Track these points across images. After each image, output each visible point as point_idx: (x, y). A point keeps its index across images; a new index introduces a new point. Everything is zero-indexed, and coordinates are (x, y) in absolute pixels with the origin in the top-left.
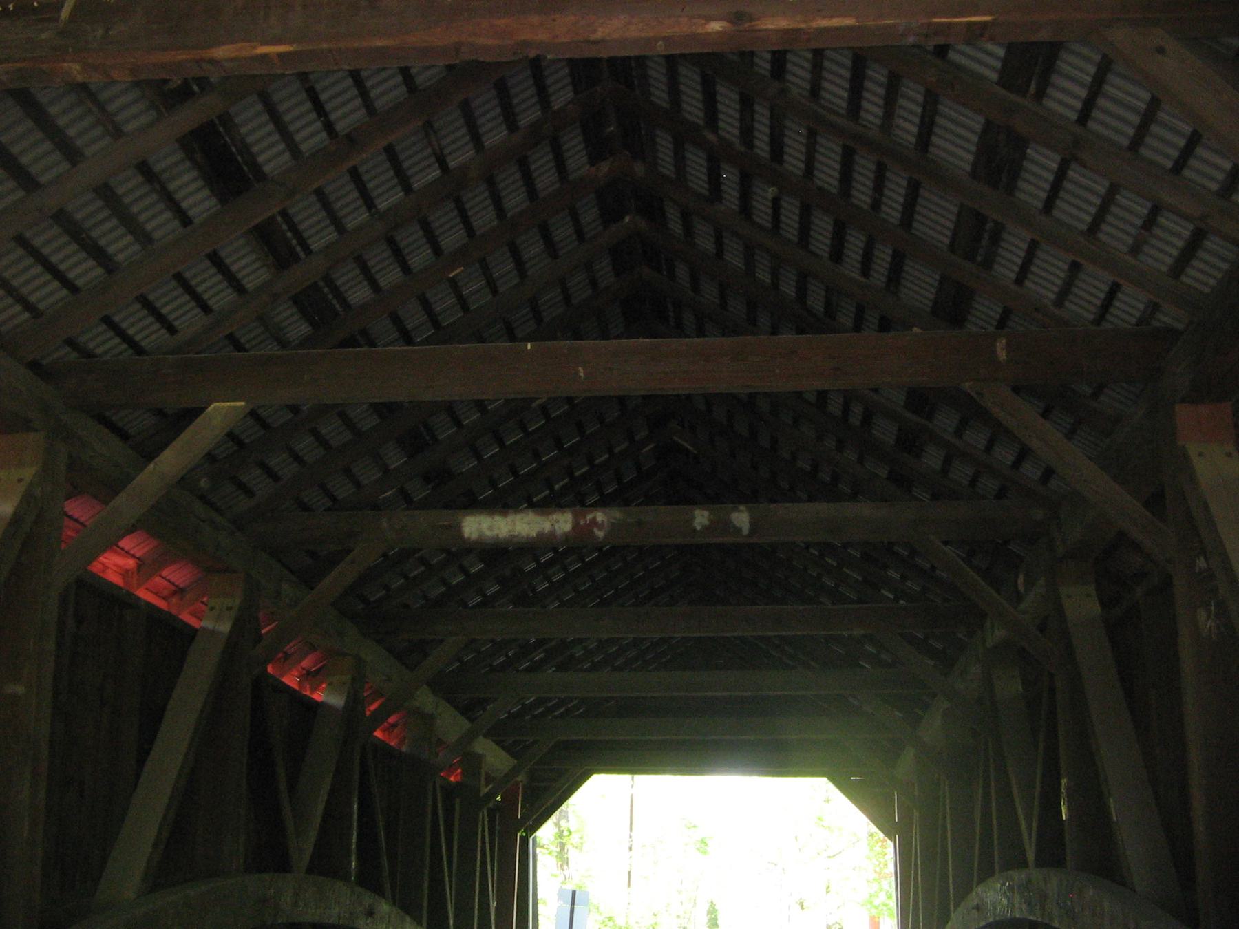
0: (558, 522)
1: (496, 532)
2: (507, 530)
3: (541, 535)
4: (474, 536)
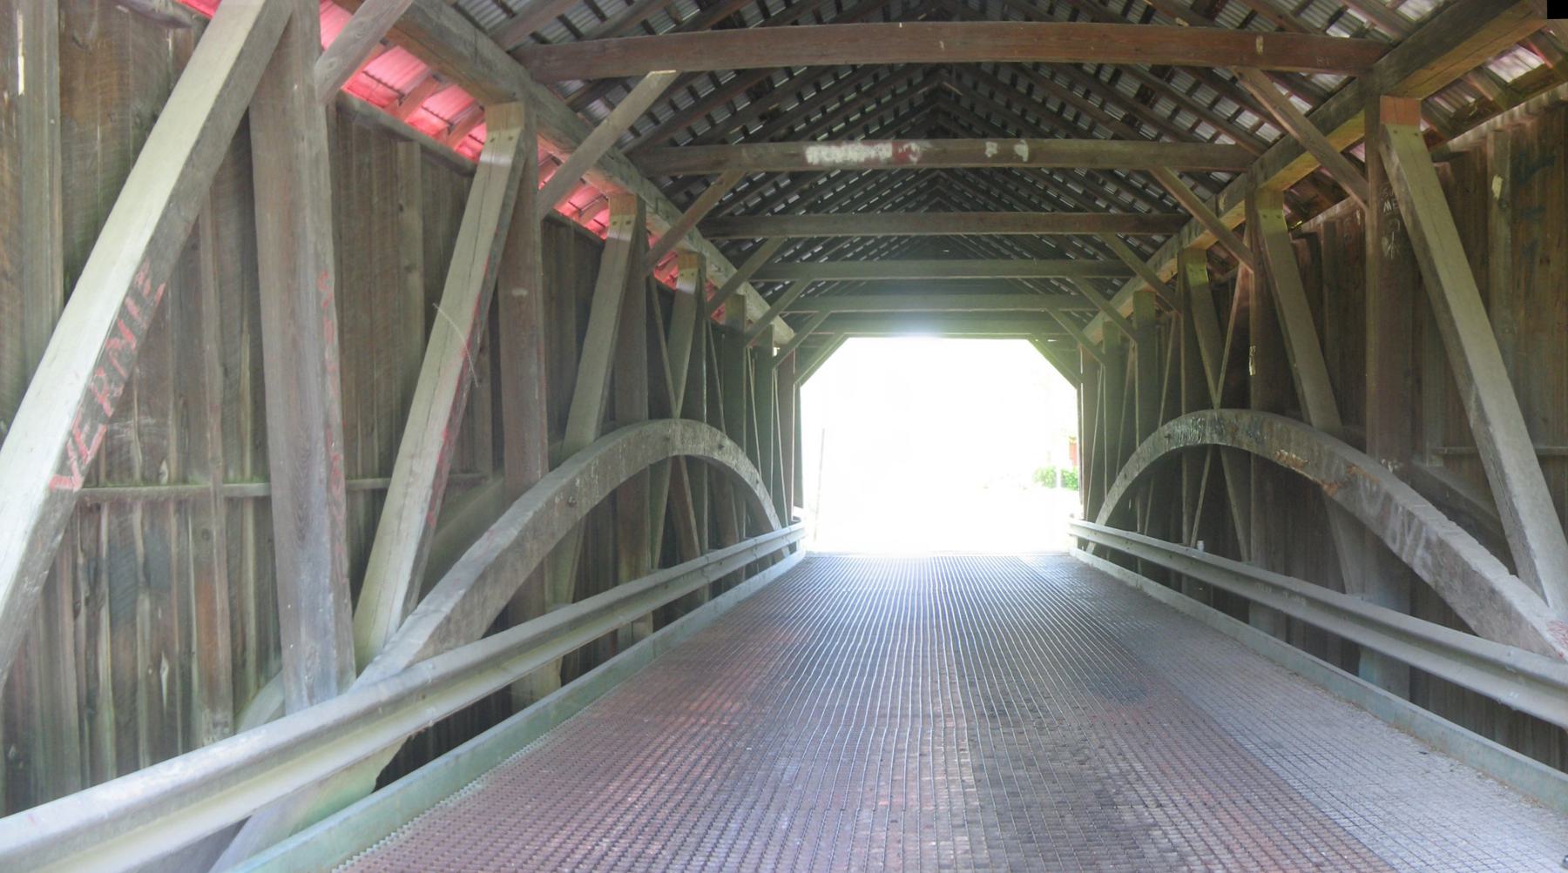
1: (833, 158)
3: (868, 161)
4: (816, 161)
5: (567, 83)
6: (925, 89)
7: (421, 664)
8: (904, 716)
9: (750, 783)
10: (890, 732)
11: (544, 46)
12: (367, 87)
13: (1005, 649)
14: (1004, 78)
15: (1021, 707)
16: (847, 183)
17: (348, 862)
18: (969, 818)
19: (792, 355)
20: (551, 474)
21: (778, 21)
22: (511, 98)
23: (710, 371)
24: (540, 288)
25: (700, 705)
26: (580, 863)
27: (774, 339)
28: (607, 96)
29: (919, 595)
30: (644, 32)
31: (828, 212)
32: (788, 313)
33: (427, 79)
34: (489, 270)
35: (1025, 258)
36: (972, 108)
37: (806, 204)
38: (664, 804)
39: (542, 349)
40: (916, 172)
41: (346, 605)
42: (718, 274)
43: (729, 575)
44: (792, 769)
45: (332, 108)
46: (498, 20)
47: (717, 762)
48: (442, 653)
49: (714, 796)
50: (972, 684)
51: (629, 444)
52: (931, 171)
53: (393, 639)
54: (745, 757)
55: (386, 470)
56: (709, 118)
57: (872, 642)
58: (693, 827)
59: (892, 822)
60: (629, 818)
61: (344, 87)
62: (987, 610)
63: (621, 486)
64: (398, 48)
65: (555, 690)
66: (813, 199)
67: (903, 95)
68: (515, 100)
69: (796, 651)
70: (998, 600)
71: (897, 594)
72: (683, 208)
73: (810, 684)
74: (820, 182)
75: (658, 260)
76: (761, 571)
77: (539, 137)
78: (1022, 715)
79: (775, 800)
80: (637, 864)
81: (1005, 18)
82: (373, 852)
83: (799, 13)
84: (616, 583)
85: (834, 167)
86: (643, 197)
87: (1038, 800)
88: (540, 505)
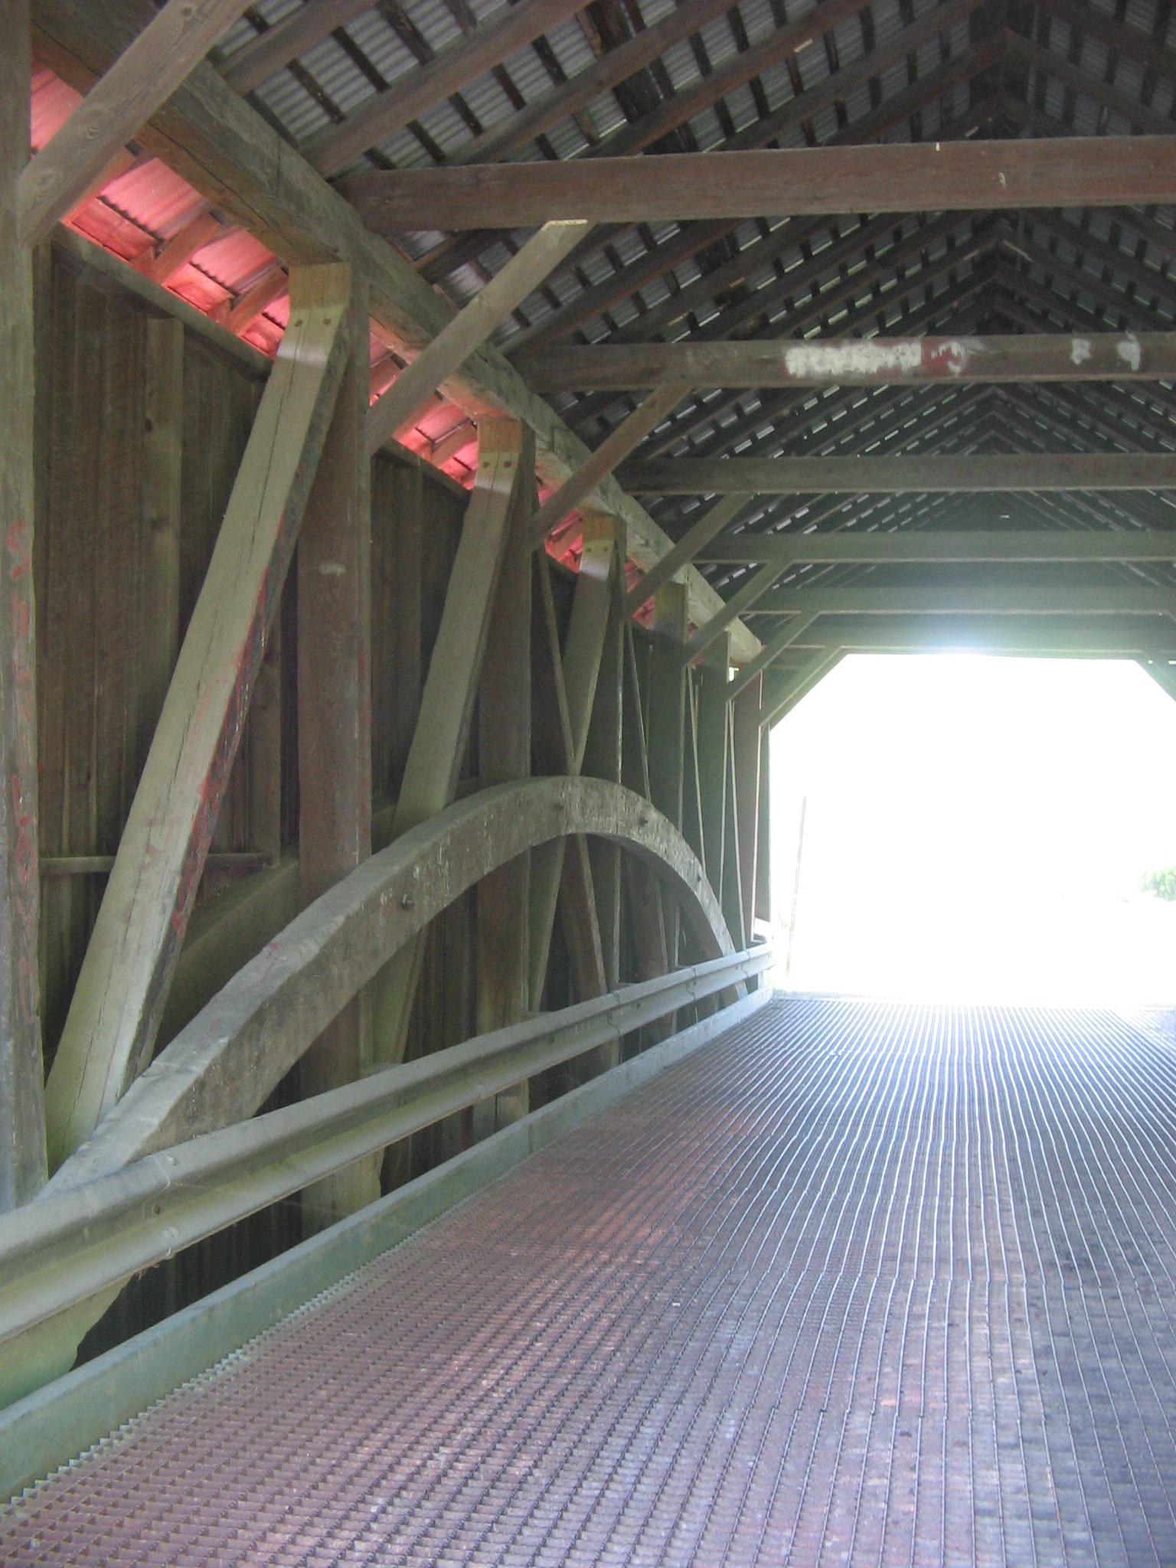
0: (903, 354)
1: (828, 367)
2: (841, 364)
3: (883, 372)
5: (419, 234)
6: (975, 253)
7: (155, 1158)
8: (924, 1260)
9: (677, 1360)
10: (902, 1285)
11: (387, 172)
12: (105, 223)
13: (1090, 1161)
14: (1100, 231)
15: (1114, 1256)
16: (848, 407)
17: (27, 1491)
18: (1027, 1435)
19: (757, 680)
20: (376, 857)
21: (747, 141)
22: (332, 257)
23: (628, 703)
24: (366, 563)
25: (600, 1232)
26: (403, 1488)
27: (730, 654)
28: (481, 258)
29: (951, 1064)
30: (540, 155)
31: (818, 454)
32: (753, 614)
33: (200, 218)
34: (284, 530)
35: (1132, 527)
36: (1049, 283)
37: (784, 441)
38: (539, 1391)
39: (367, 662)
40: (958, 389)
41: (35, 1059)
42: (646, 550)
43: (650, 1025)
44: (742, 1341)
45: (44, 252)
46: (316, 126)
47: (625, 1325)
48: (191, 1138)
49: (619, 1381)
50: (1036, 1213)
51: (499, 812)
52: (981, 387)
53: (109, 1116)
54: (670, 1317)
55: (109, 843)
56: (638, 301)
57: (875, 1138)
58: (584, 1432)
59: (903, 1434)
60: (482, 1413)
61: (66, 221)
62: (1062, 1095)
63: (484, 880)
64: (156, 161)
65: (371, 1202)
66: (796, 433)
67: (942, 262)
68: (337, 260)
69: (754, 1148)
70: (1081, 1078)
71: (917, 1062)
72: (593, 443)
73: (776, 1202)
74: (807, 407)
75: (550, 526)
76: (700, 1020)
77: (371, 320)
78: (1117, 1269)
79: (716, 1391)
80: (493, 1492)
81: (1101, 131)
82: (68, 1473)
83: (780, 127)
84: (473, 1032)
85: (828, 381)
86: (532, 425)
87: (1140, 1412)
88: (356, 905)
